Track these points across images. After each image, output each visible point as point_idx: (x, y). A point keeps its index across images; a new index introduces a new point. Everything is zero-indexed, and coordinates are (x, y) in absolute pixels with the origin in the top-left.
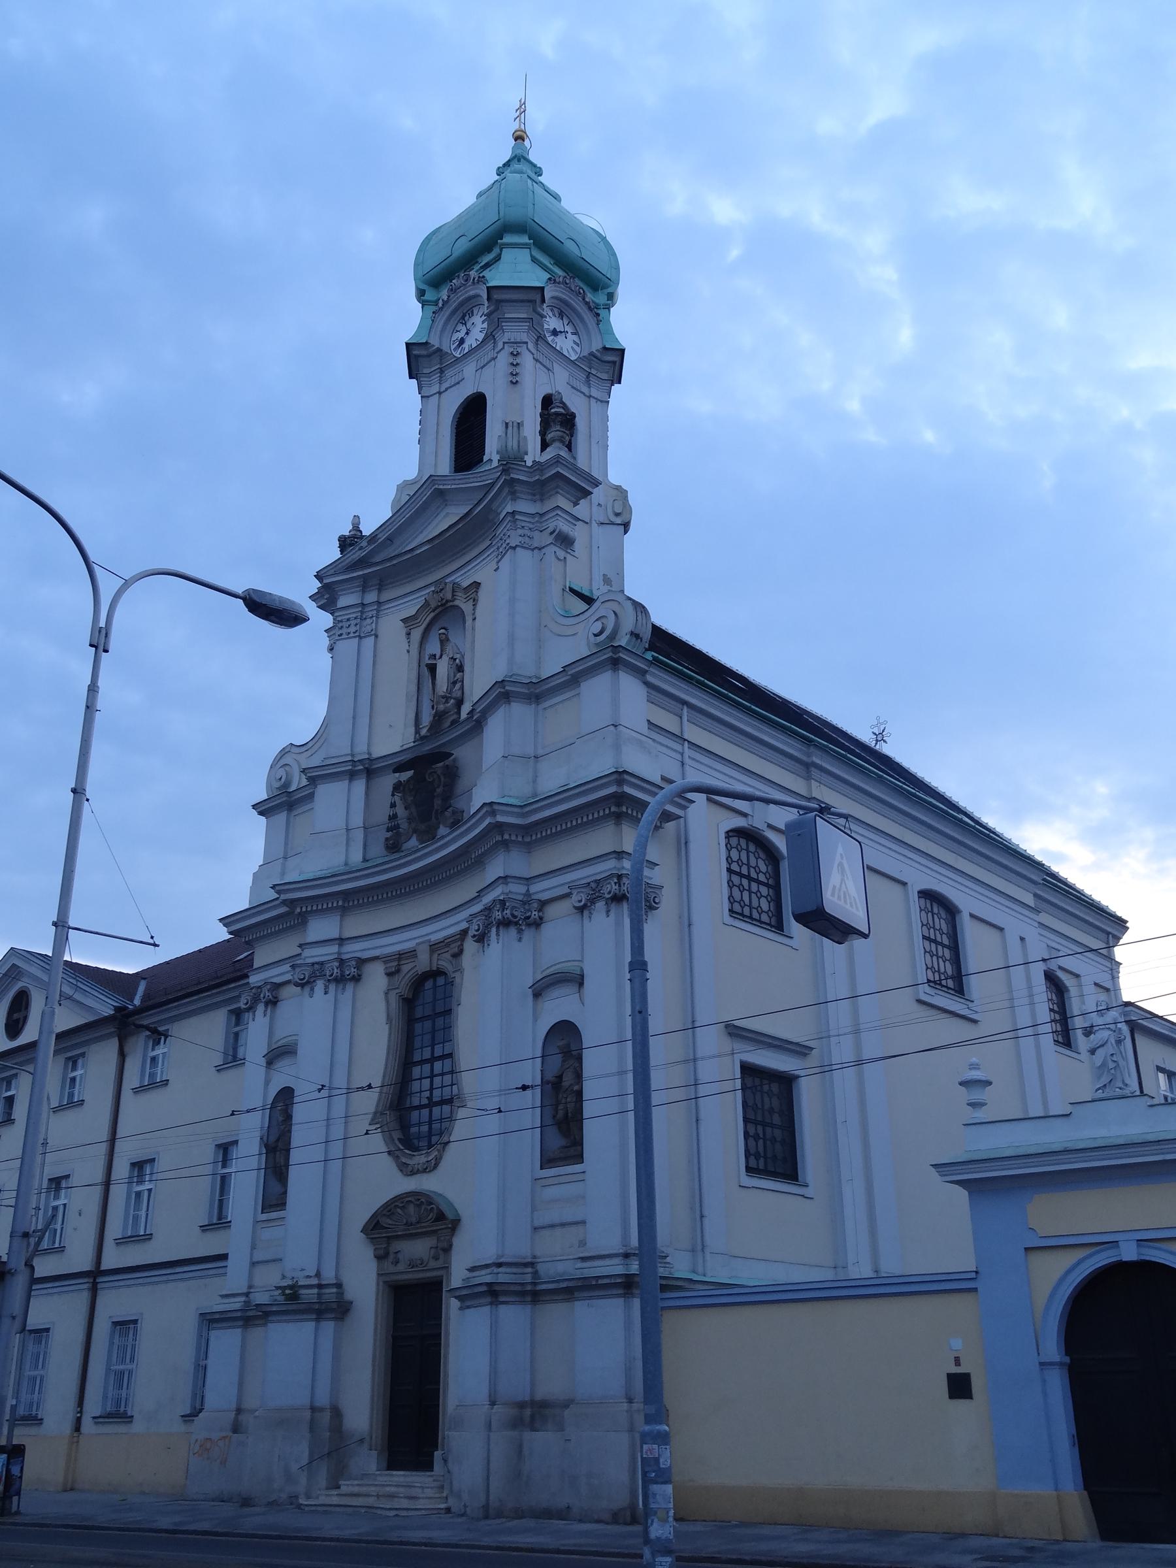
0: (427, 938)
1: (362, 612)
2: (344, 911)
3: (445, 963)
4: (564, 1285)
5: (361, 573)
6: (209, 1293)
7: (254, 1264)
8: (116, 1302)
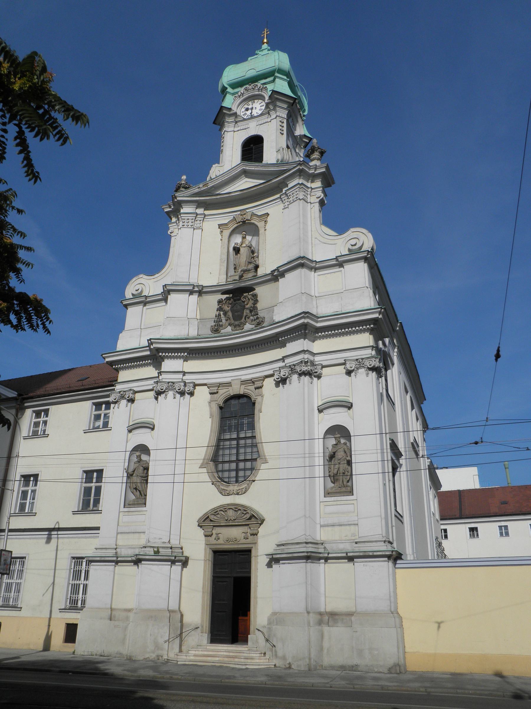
0: (240, 377)
2: (186, 359)
3: (250, 390)
4: (306, 554)
6: (87, 546)
7: (118, 533)
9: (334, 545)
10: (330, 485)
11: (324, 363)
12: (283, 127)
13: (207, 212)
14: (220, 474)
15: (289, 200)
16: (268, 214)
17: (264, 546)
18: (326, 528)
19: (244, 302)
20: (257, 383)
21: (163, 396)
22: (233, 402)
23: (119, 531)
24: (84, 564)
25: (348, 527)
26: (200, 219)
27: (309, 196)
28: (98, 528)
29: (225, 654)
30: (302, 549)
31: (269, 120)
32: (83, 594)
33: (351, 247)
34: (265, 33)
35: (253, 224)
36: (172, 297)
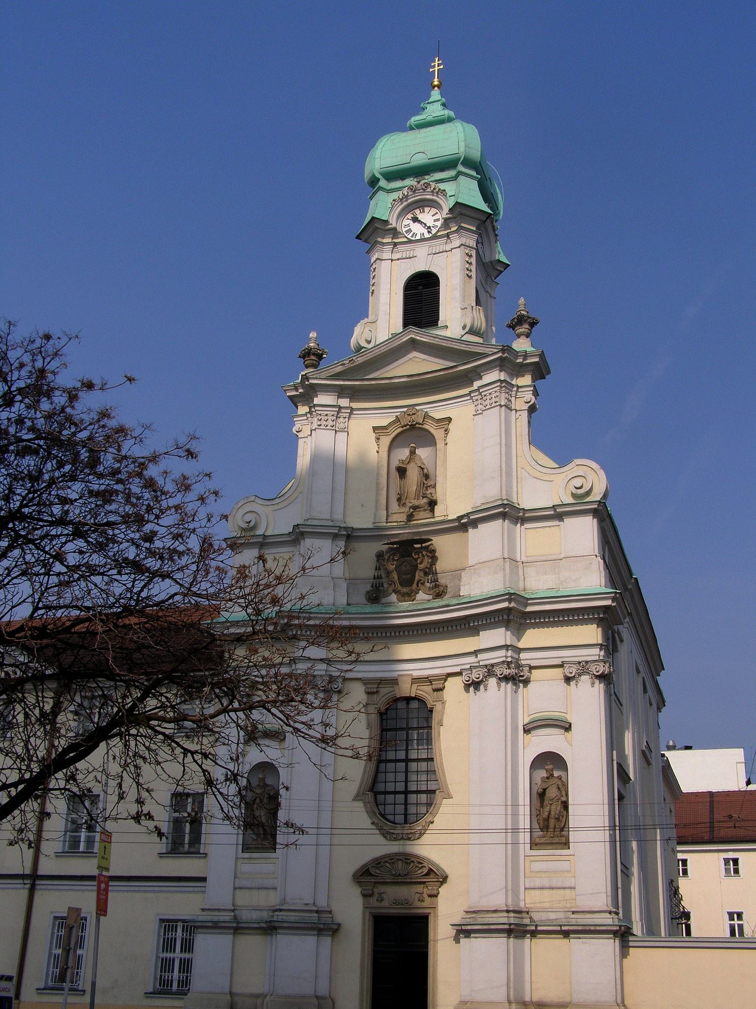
1: (338, 412)
3: (425, 691)
5: (342, 383)
6: (184, 904)
7: (235, 888)
11: (534, 663)
12: (471, 264)
13: (355, 405)
14: (381, 807)
15: (485, 403)
16: (449, 419)
17: (447, 911)
18: (532, 892)
19: (416, 560)
20: (437, 683)
23: (237, 886)
24: (180, 930)
25: (562, 891)
26: (344, 415)
27: (513, 399)
28: (204, 879)
30: (502, 918)
31: (448, 247)
32: (180, 972)
33: (574, 491)
34: (437, 66)
35: (427, 430)
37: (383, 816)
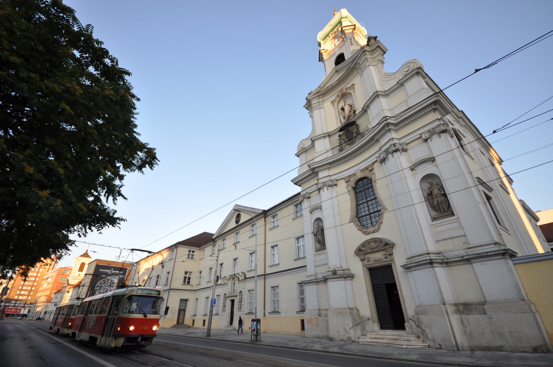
3: (367, 174)
6: (302, 276)
8: (271, 282)
9: (450, 253)
10: (434, 214)
17: (399, 260)
20: (370, 169)
21: (322, 190)
22: (360, 183)
28: (306, 266)
29: (391, 337)
36: (317, 143)
37: (363, 226)
